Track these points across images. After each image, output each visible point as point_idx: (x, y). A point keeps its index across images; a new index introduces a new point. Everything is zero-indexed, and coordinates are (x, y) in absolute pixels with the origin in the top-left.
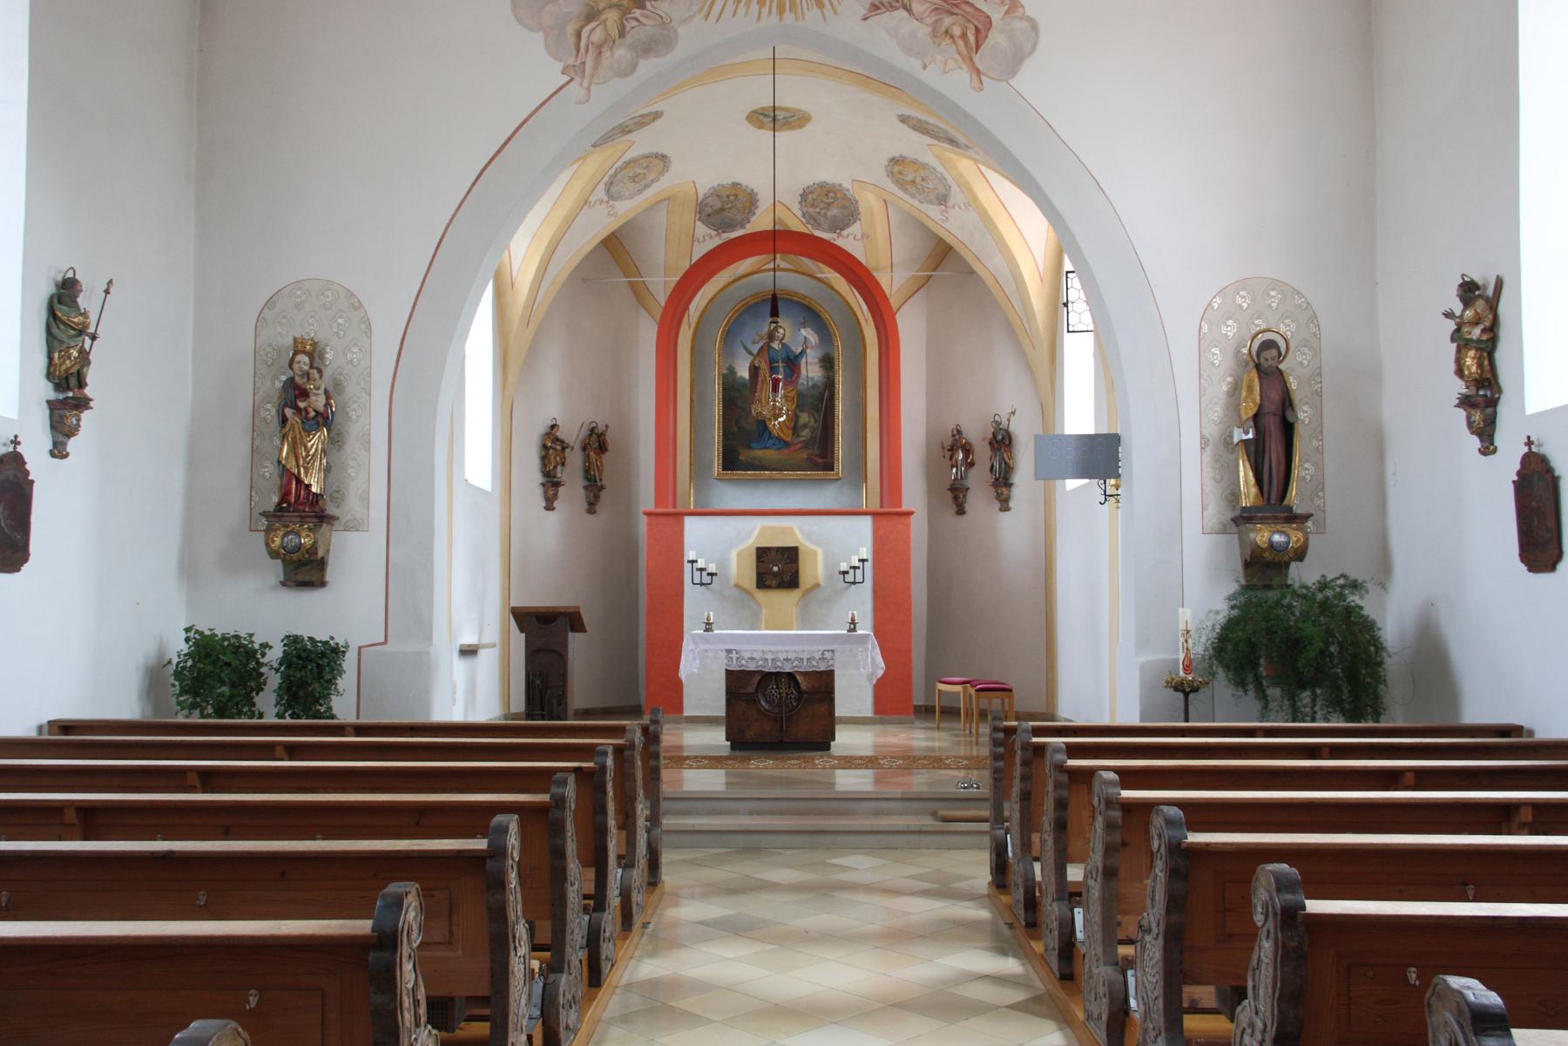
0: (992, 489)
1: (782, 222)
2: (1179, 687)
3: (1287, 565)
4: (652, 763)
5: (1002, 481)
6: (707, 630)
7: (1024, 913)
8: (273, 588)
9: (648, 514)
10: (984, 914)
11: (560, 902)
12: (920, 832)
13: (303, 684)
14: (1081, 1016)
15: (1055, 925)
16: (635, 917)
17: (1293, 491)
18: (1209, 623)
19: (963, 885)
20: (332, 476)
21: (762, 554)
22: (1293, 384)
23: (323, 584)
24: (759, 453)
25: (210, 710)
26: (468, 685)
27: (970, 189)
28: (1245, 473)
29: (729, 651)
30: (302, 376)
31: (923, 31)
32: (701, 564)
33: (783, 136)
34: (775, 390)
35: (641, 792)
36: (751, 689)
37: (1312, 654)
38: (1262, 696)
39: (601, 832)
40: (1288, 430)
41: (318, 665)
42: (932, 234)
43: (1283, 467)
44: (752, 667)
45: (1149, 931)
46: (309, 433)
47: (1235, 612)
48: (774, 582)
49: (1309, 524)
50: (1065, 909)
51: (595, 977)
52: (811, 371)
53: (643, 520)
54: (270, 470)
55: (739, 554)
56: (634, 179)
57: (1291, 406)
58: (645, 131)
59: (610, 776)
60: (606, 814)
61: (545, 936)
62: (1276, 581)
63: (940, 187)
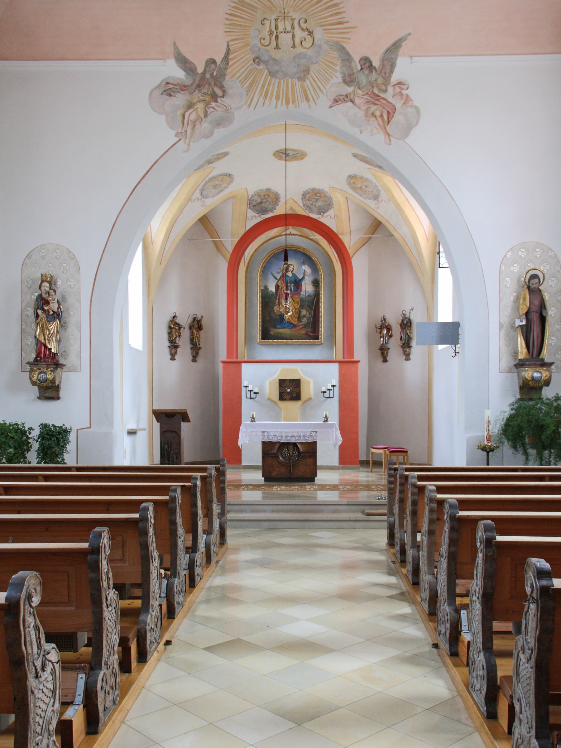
0: (401, 349)
1: (291, 209)
2: (484, 449)
3: (541, 388)
4: (222, 486)
5: (406, 345)
6: (252, 421)
7: (401, 554)
8: (34, 400)
9: (223, 362)
10: (382, 557)
11: (174, 545)
12: (356, 521)
13: (50, 447)
14: (419, 600)
15: (411, 560)
16: (213, 558)
17: (545, 352)
18: (501, 417)
19: (374, 545)
20: (62, 344)
21: (282, 382)
22: (546, 296)
23: (59, 398)
24: (281, 331)
25: (4, 460)
26: (132, 447)
27: (391, 192)
28: (521, 341)
29: (263, 432)
30: (46, 293)
31: (361, 113)
32: (250, 388)
33: (291, 165)
34: (286, 299)
35: (215, 499)
36: (275, 451)
37: (549, 432)
38: (526, 453)
39: (195, 516)
40: (543, 320)
41: (57, 438)
42: (372, 216)
43: (540, 336)
44: (275, 440)
45: (443, 556)
46: (50, 322)
47: (513, 412)
48: (288, 397)
49: (553, 367)
50: (416, 552)
51: (192, 583)
52: (307, 288)
53: (221, 365)
54: (31, 341)
55: (270, 383)
56: (214, 187)
57: (545, 308)
58: (220, 162)
59: (198, 490)
60: (197, 507)
61: (167, 564)
62: (535, 396)
63: (375, 191)
